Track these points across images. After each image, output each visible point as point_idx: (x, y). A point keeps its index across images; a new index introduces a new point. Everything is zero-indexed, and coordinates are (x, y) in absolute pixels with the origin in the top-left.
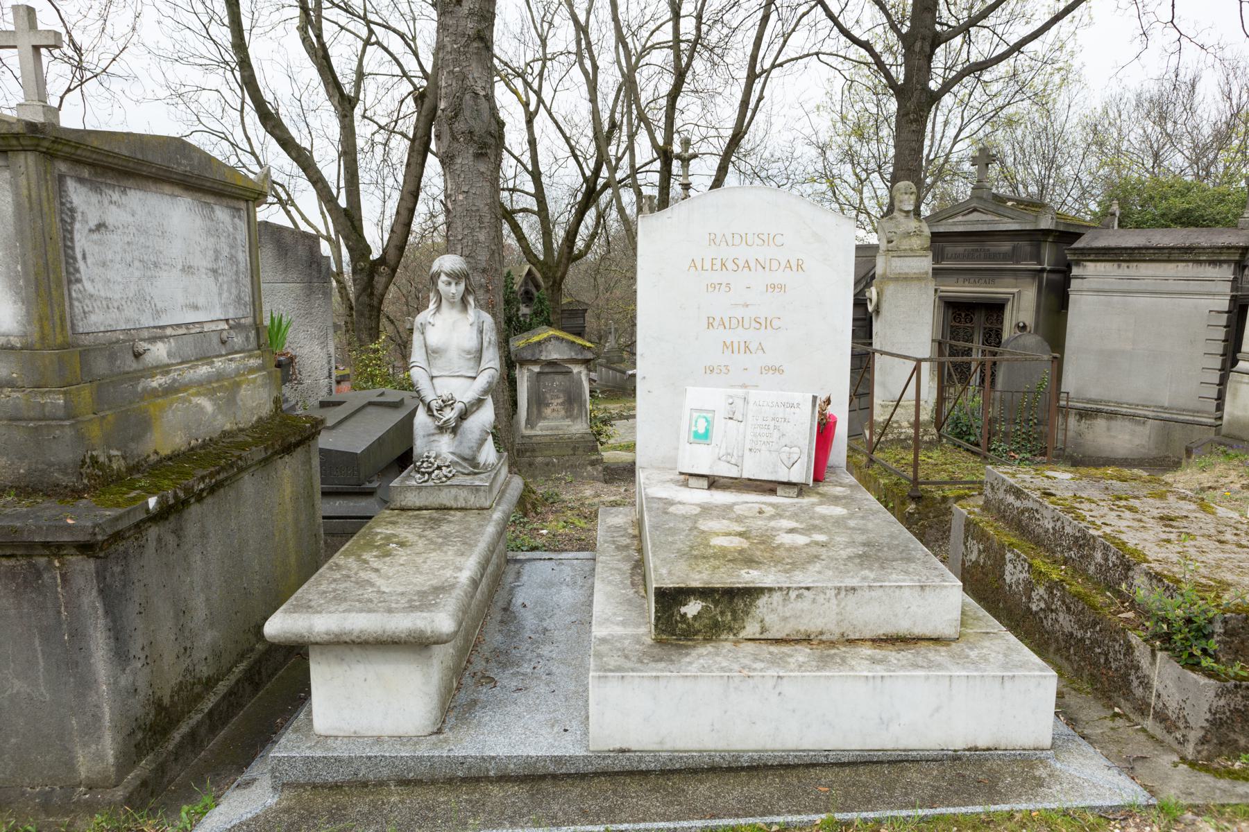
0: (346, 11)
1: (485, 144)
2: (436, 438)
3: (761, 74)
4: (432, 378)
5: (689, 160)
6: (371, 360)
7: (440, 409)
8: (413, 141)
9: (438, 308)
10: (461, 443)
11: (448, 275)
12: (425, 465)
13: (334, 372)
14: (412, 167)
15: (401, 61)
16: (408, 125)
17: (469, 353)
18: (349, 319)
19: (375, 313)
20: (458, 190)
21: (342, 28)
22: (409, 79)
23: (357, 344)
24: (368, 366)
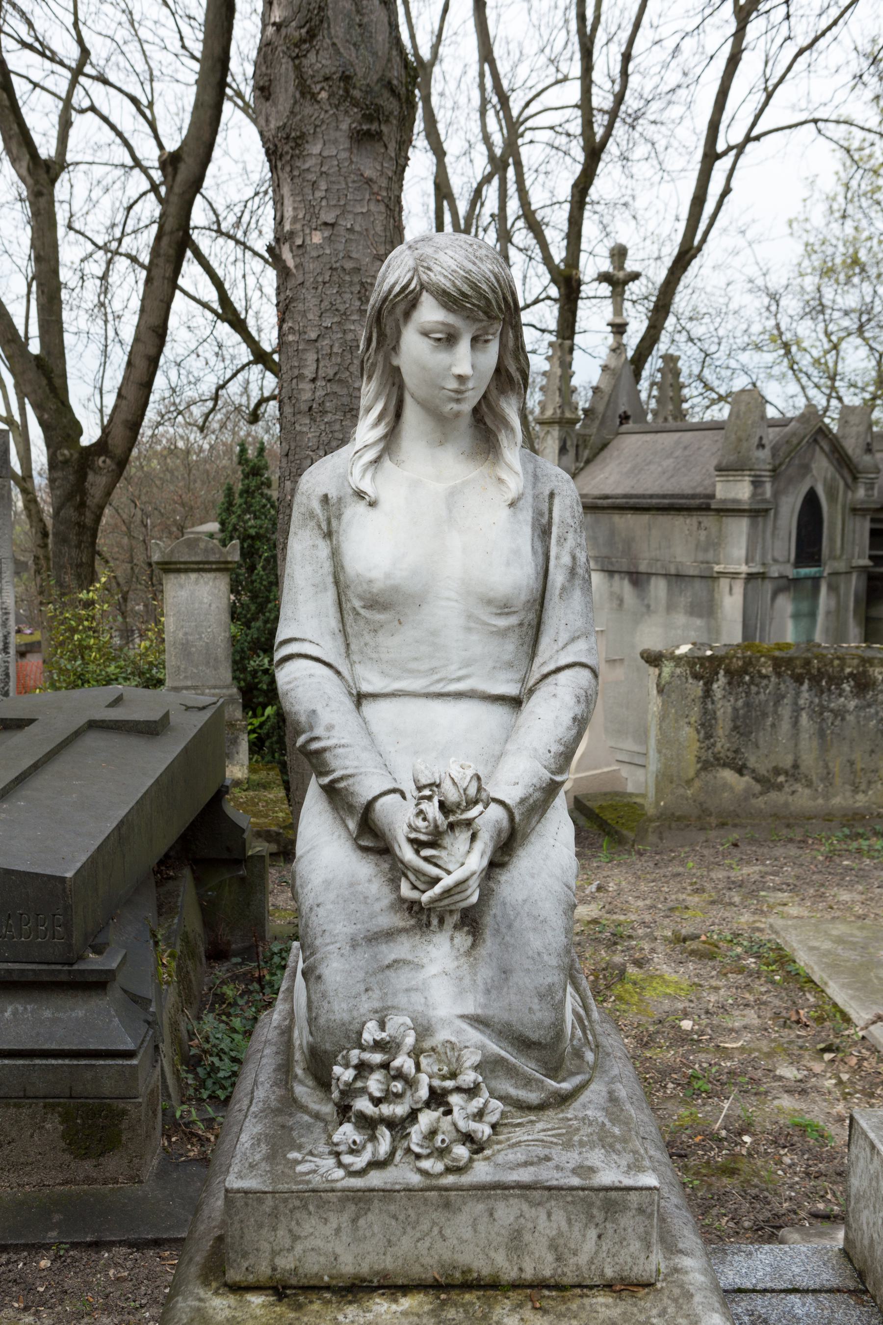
0: (43, 55)
1: (378, 108)
2: (401, 949)
3: (725, 153)
4: (360, 698)
5: (626, 282)
6: (80, 620)
7: (431, 841)
8: (149, 269)
9: (390, 441)
10: (505, 972)
11: (449, 300)
12: (375, 1084)
13: (14, 639)
14: (156, 283)
15: (132, 142)
16: (142, 244)
17: (504, 608)
18: (40, 553)
19: (87, 538)
20: (311, 217)
21: (36, 85)
22: (145, 170)
23: (55, 592)
24: (74, 631)
